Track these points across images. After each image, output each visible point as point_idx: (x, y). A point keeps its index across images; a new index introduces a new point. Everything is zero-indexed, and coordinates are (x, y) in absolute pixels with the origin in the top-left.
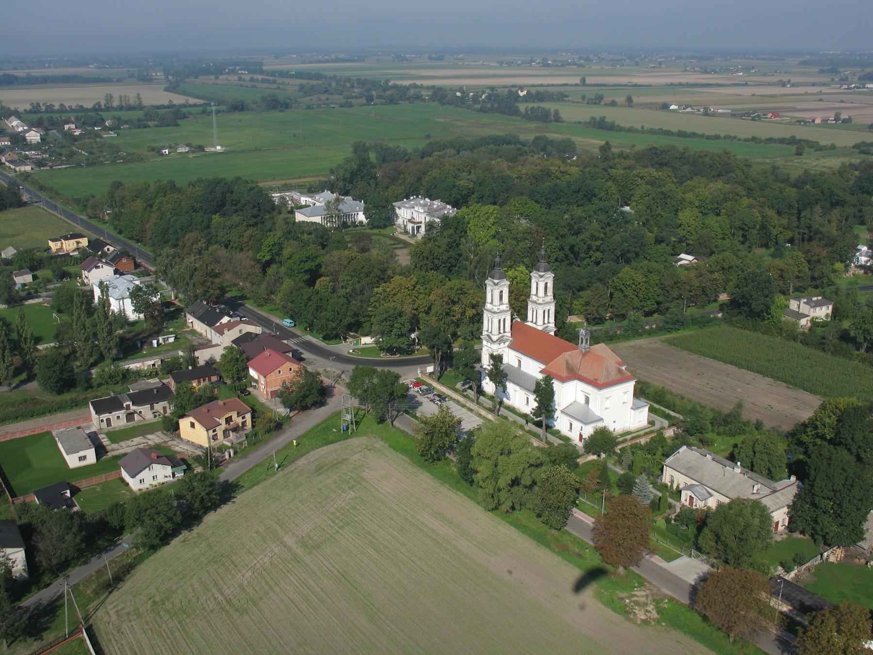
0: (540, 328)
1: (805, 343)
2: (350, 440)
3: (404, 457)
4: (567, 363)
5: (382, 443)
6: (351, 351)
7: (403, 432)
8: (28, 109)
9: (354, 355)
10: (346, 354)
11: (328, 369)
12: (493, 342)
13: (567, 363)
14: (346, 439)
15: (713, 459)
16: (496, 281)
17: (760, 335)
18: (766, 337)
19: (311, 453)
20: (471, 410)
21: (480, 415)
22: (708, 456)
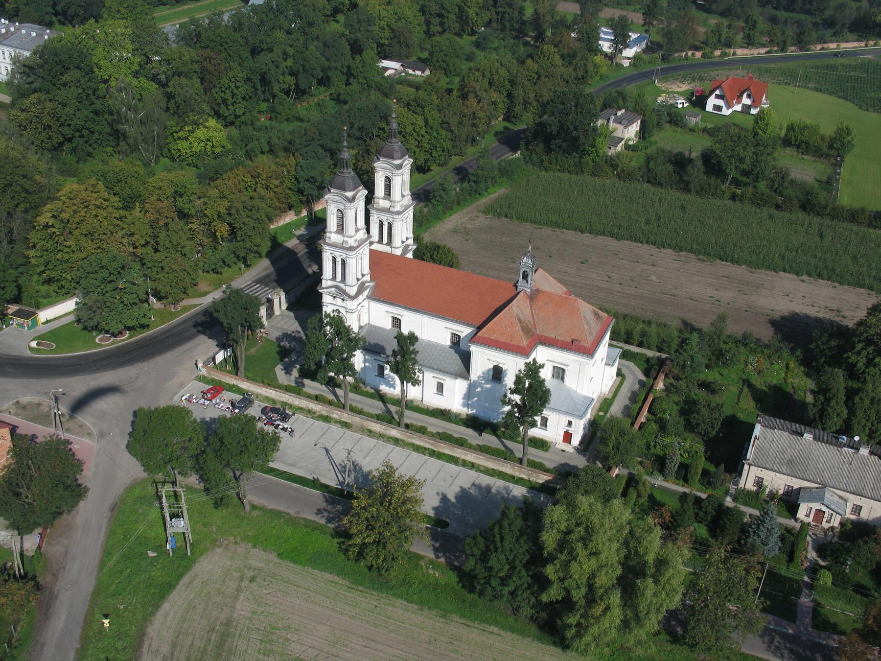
0: (398, 252)
1: (625, 175)
2: (197, 568)
3: (330, 577)
4: (519, 319)
5: (262, 554)
6: (34, 344)
7: (278, 514)
8: (199, 321)
9: (46, 352)
10: (28, 353)
11: (25, 400)
12: (353, 298)
13: (519, 319)
14: (187, 568)
15: (871, 453)
16: (349, 194)
17: (589, 179)
18: (598, 181)
19: (151, 631)
20: (346, 425)
21: (370, 431)
22: (806, 435)
